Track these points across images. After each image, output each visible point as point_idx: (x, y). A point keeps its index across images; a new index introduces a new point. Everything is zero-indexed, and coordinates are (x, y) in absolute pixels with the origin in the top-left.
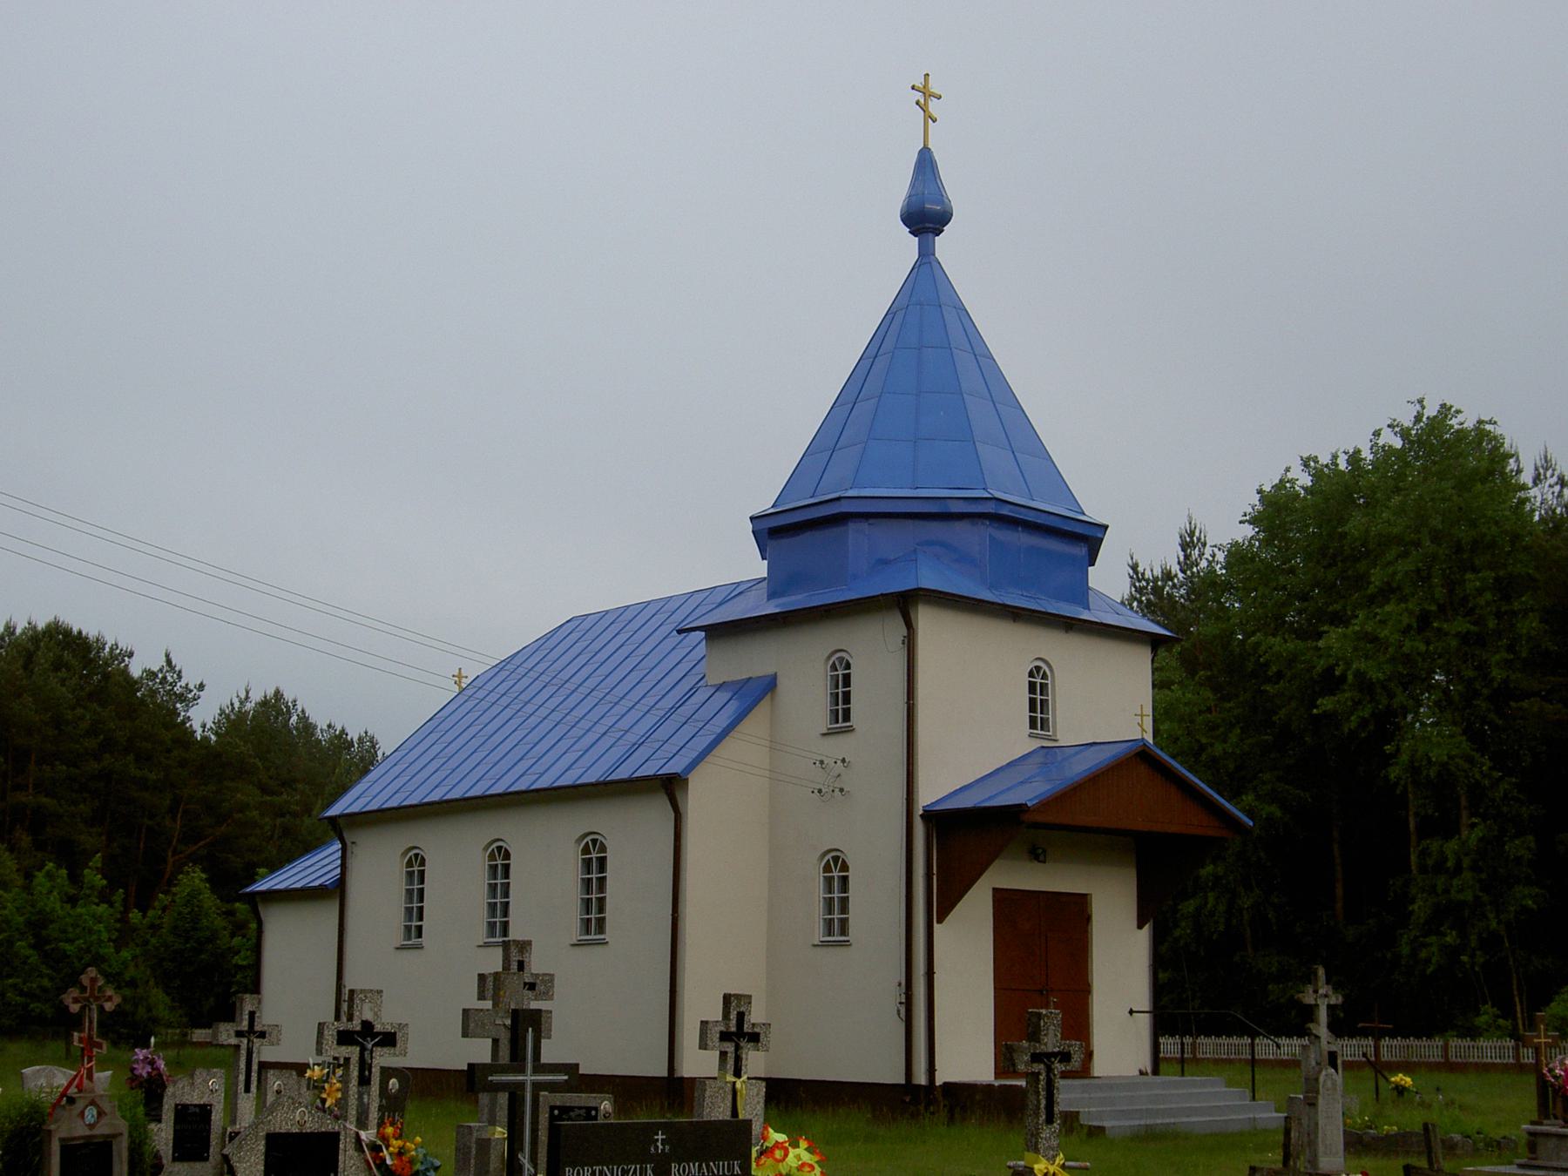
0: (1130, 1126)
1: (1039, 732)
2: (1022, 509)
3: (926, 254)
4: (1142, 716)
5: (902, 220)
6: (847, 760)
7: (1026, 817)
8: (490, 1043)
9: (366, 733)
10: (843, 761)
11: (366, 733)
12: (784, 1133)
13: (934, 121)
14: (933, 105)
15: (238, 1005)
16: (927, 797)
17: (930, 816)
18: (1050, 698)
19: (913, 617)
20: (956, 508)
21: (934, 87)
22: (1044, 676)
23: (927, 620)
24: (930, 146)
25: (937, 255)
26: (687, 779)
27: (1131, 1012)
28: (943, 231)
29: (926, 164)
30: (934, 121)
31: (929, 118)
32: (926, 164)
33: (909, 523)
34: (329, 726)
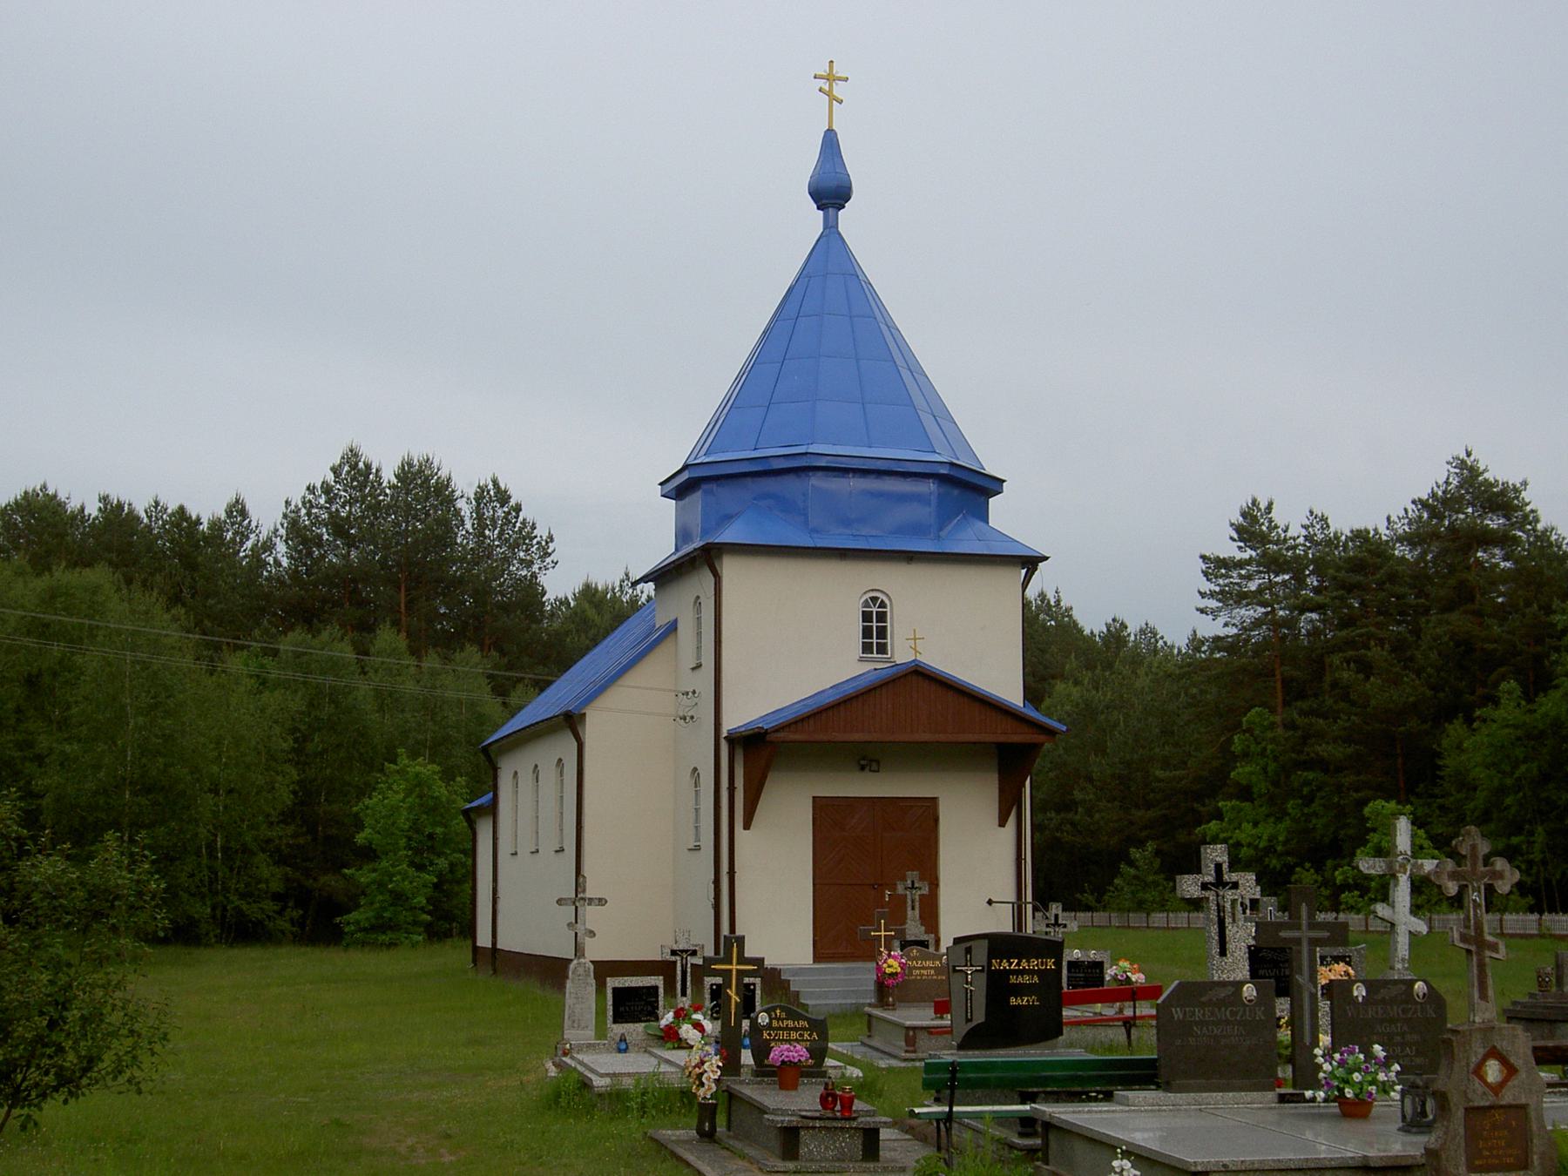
0: (840, 1004)
1: (875, 655)
2: (844, 459)
3: (831, 227)
4: (915, 639)
5: (810, 193)
6: (697, 692)
7: (768, 738)
8: (737, 930)
9: (1147, 624)
10: (694, 692)
11: (1147, 624)
12: (987, 1014)
13: (841, 102)
14: (839, 89)
15: (1392, 885)
16: (733, 720)
17: (733, 740)
18: (888, 624)
19: (718, 569)
20: (777, 465)
21: (839, 71)
22: (883, 605)
23: (730, 568)
24: (834, 128)
25: (840, 229)
26: (585, 714)
27: (990, 902)
28: (844, 207)
29: (830, 143)
30: (841, 102)
31: (832, 98)
32: (830, 143)
33: (749, 481)
34: (1114, 620)
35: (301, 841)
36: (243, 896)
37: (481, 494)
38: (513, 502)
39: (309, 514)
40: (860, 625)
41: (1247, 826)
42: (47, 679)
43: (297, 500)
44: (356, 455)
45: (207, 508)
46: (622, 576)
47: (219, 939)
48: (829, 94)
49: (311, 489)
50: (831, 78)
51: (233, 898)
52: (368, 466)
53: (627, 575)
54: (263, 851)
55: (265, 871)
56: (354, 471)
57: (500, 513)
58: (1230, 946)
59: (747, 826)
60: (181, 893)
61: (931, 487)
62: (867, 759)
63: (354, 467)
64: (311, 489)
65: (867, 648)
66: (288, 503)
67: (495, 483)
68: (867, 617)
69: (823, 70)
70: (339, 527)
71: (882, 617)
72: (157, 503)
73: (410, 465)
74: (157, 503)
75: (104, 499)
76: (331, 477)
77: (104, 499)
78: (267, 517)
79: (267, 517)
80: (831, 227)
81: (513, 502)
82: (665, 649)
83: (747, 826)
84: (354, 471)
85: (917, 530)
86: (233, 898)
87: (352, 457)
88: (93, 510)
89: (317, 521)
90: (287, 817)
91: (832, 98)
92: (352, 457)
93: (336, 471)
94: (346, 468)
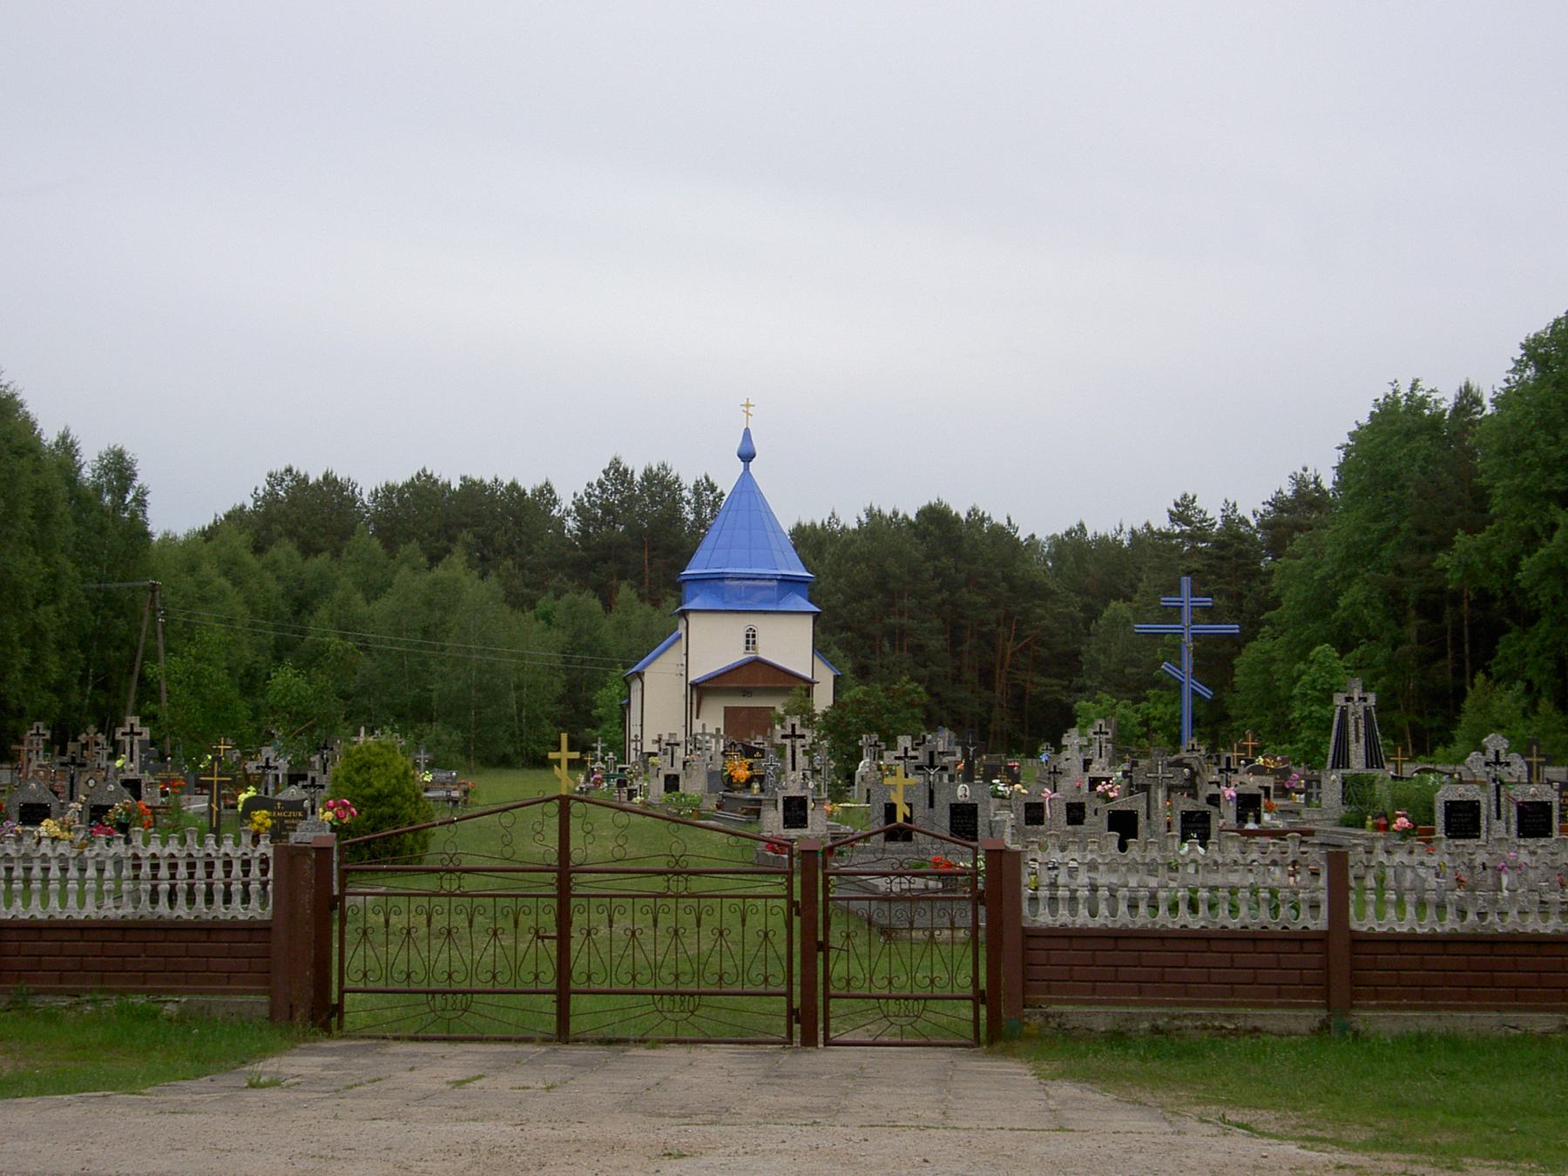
3: (747, 468)
17: (694, 685)
21: (751, 402)
23: (692, 618)
29: (747, 433)
31: (748, 414)
32: (747, 433)
35: (569, 713)
36: (536, 742)
37: (697, 491)
38: (718, 491)
39: (589, 501)
40: (745, 639)
41: (1160, 706)
42: (432, 629)
43: (581, 493)
44: (618, 463)
45: (528, 485)
46: (830, 515)
47: (524, 766)
48: (747, 412)
49: (590, 485)
50: (748, 405)
51: (531, 743)
52: (626, 470)
53: (833, 514)
54: (547, 718)
55: (548, 730)
56: (618, 473)
57: (711, 498)
58: (797, 766)
59: (697, 718)
60: (1381, 606)
61: (775, 583)
62: (746, 692)
63: (617, 470)
64: (590, 485)
65: (747, 648)
66: (575, 495)
67: (707, 479)
68: (748, 636)
69: (745, 402)
70: (608, 509)
71: (754, 636)
72: (496, 480)
73: (651, 470)
74: (496, 480)
75: (464, 478)
76: (603, 476)
77: (464, 478)
78: (566, 499)
79: (566, 499)
80: (747, 468)
81: (718, 491)
82: (676, 645)
83: (697, 718)
84: (618, 473)
85: (770, 601)
86: (531, 743)
87: (615, 464)
88: (456, 485)
89: (593, 505)
90: (560, 701)
91: (748, 414)
92: (615, 464)
93: (606, 473)
94: (612, 471)
